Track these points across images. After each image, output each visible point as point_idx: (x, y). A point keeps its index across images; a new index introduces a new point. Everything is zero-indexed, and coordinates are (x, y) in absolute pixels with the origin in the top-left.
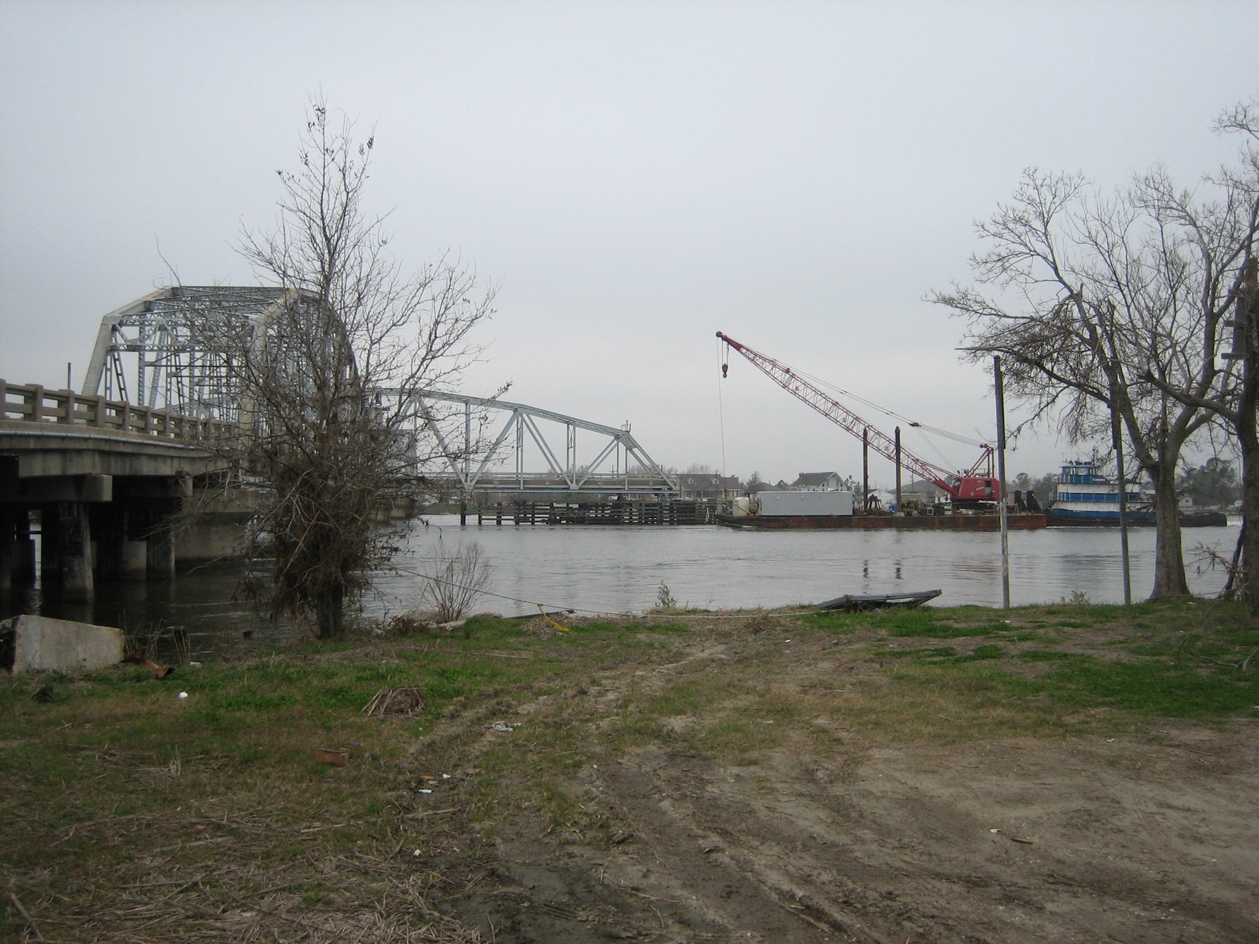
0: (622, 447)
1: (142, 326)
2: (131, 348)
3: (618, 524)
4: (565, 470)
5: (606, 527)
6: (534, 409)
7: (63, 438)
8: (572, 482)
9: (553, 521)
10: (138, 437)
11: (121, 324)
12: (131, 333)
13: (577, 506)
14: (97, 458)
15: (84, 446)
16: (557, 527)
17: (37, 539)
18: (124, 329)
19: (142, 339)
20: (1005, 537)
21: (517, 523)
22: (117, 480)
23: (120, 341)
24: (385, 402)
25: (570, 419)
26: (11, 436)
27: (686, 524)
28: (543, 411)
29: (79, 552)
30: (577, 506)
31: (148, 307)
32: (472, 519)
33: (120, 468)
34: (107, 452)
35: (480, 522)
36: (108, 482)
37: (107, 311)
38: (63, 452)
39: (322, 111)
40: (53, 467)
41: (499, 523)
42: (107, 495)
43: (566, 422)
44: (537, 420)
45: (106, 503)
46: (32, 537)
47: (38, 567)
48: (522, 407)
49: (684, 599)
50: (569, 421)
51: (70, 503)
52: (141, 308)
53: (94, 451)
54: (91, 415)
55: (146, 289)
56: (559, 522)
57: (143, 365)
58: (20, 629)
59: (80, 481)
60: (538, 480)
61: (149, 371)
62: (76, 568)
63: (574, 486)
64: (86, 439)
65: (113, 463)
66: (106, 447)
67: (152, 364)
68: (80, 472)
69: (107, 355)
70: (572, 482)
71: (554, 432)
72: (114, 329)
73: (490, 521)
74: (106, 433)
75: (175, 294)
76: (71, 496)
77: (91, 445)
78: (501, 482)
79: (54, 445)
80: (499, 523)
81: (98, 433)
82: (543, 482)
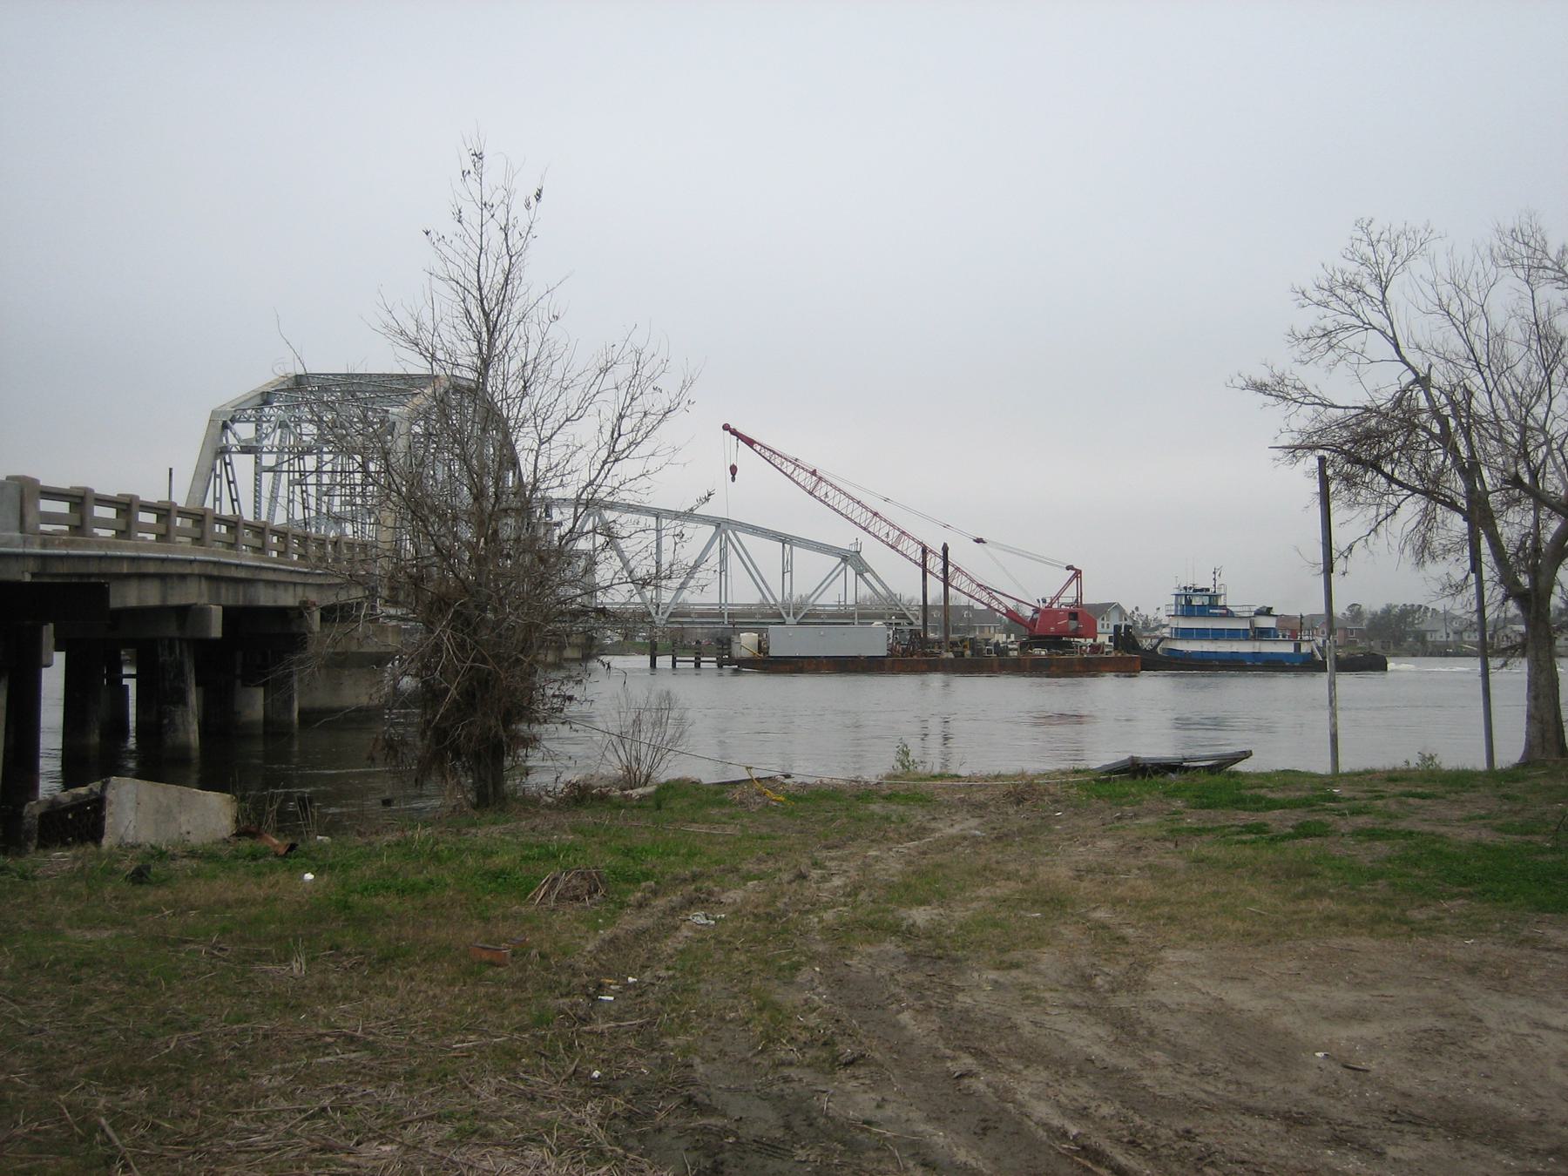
0: (851, 571)
2: (246, 450)
6: (741, 524)
7: (163, 560)
8: (788, 615)
10: (254, 559)
11: (233, 420)
12: (246, 431)
14: (204, 584)
15: (187, 570)
17: (131, 684)
18: (237, 427)
19: (259, 439)
24: (556, 515)
25: (786, 536)
26: (100, 558)
29: (181, 699)
31: (266, 399)
32: (664, 661)
33: (231, 597)
34: (215, 578)
36: (217, 613)
38: (162, 577)
40: (150, 595)
41: (698, 665)
43: (781, 540)
45: (216, 641)
46: (125, 681)
48: (728, 521)
50: (784, 539)
51: (171, 640)
52: (258, 401)
53: (200, 576)
58: (110, 794)
61: (267, 478)
62: (178, 720)
64: (191, 562)
67: (270, 470)
68: (183, 602)
70: (788, 615)
71: (766, 554)
72: (225, 426)
73: (686, 664)
74: (214, 554)
75: (299, 382)
76: (172, 630)
77: (196, 569)
79: (151, 568)
80: (698, 665)
81: (206, 553)
82: (752, 615)
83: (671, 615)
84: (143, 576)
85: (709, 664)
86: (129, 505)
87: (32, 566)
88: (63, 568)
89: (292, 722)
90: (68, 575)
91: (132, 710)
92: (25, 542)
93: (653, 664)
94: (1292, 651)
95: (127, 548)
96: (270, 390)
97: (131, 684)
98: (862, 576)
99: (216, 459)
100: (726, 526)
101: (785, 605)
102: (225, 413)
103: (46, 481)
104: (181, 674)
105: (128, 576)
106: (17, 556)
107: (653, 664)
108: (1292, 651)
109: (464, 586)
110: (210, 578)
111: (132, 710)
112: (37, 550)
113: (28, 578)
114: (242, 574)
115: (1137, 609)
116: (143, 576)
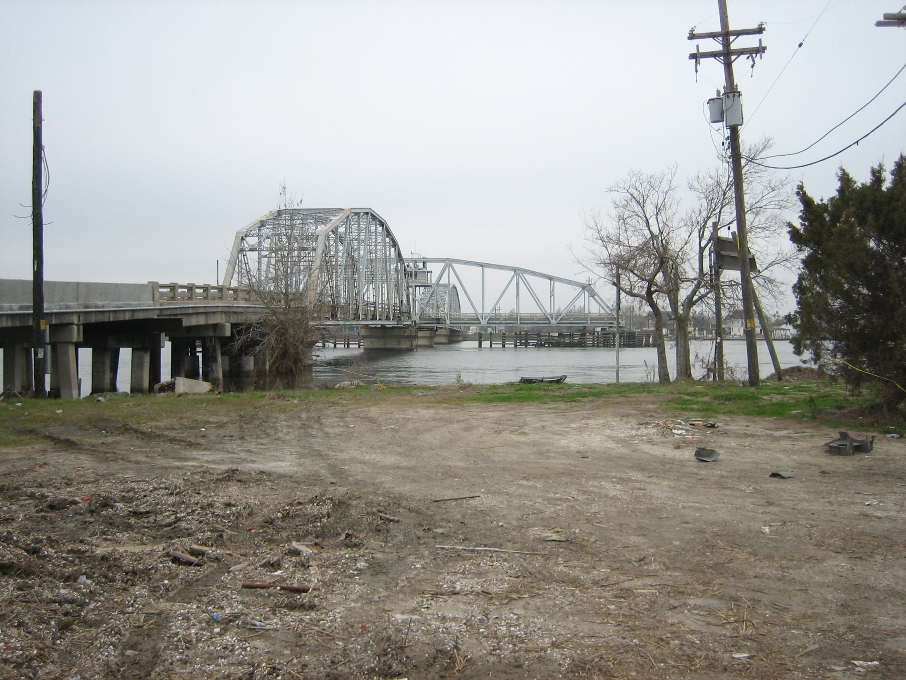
0: (587, 293)
1: (259, 236)
2: (252, 250)
3: (584, 347)
4: (548, 311)
5: (575, 348)
7: (206, 307)
8: (552, 318)
9: (539, 345)
10: (245, 304)
11: (246, 236)
12: (252, 241)
13: (557, 335)
14: (223, 315)
15: (216, 310)
16: (543, 349)
17: (200, 355)
18: (248, 239)
19: (260, 243)
20: (618, 352)
21: (516, 346)
22: (233, 326)
23: (246, 246)
24: (429, 267)
26: (181, 308)
27: (629, 347)
28: (532, 272)
29: (216, 361)
30: (557, 335)
31: (262, 224)
32: (486, 344)
33: (234, 319)
34: (227, 312)
35: (491, 346)
36: (228, 326)
37: (238, 229)
38: (206, 313)
39: (285, 188)
40: (201, 321)
41: (504, 346)
42: (228, 333)
44: (528, 277)
45: (227, 337)
46: (198, 354)
47: (201, 370)
48: (519, 269)
49: (467, 379)
50: (551, 278)
51: (211, 337)
52: (259, 225)
53: (221, 312)
54: (220, 295)
55: (264, 211)
56: (543, 346)
57: (260, 257)
58: (176, 382)
59: (215, 326)
60: (531, 319)
61: (264, 260)
62: (214, 368)
63: (553, 322)
64: (217, 307)
65: (232, 318)
66: (227, 310)
67: (265, 256)
68: (215, 322)
69: (238, 254)
70: (552, 318)
71: (541, 286)
72: (242, 239)
73: (497, 345)
74: (227, 303)
76: (211, 334)
77: (219, 310)
78: (505, 319)
79: (201, 310)
80: (504, 346)
81: (223, 303)
82: (533, 319)
83: (490, 319)
84: (197, 314)
85: (510, 345)
86: (192, 287)
87: (157, 313)
88: (168, 313)
89: (266, 369)
90: (170, 315)
91: (201, 366)
92: (154, 305)
93: (480, 345)
94: (121, 349)
95: (191, 303)
96: (264, 219)
97: (200, 355)
98: (593, 297)
99: (238, 254)
100: (519, 272)
101: (551, 314)
102: (243, 232)
103: (161, 282)
104: (215, 351)
105: (192, 314)
106: (152, 309)
107: (480, 345)
108: (121, 349)
109: (281, 322)
110: (225, 312)
111: (201, 366)
112: (159, 307)
113: (156, 317)
114: (240, 310)
115: (777, 312)
116: (197, 314)
